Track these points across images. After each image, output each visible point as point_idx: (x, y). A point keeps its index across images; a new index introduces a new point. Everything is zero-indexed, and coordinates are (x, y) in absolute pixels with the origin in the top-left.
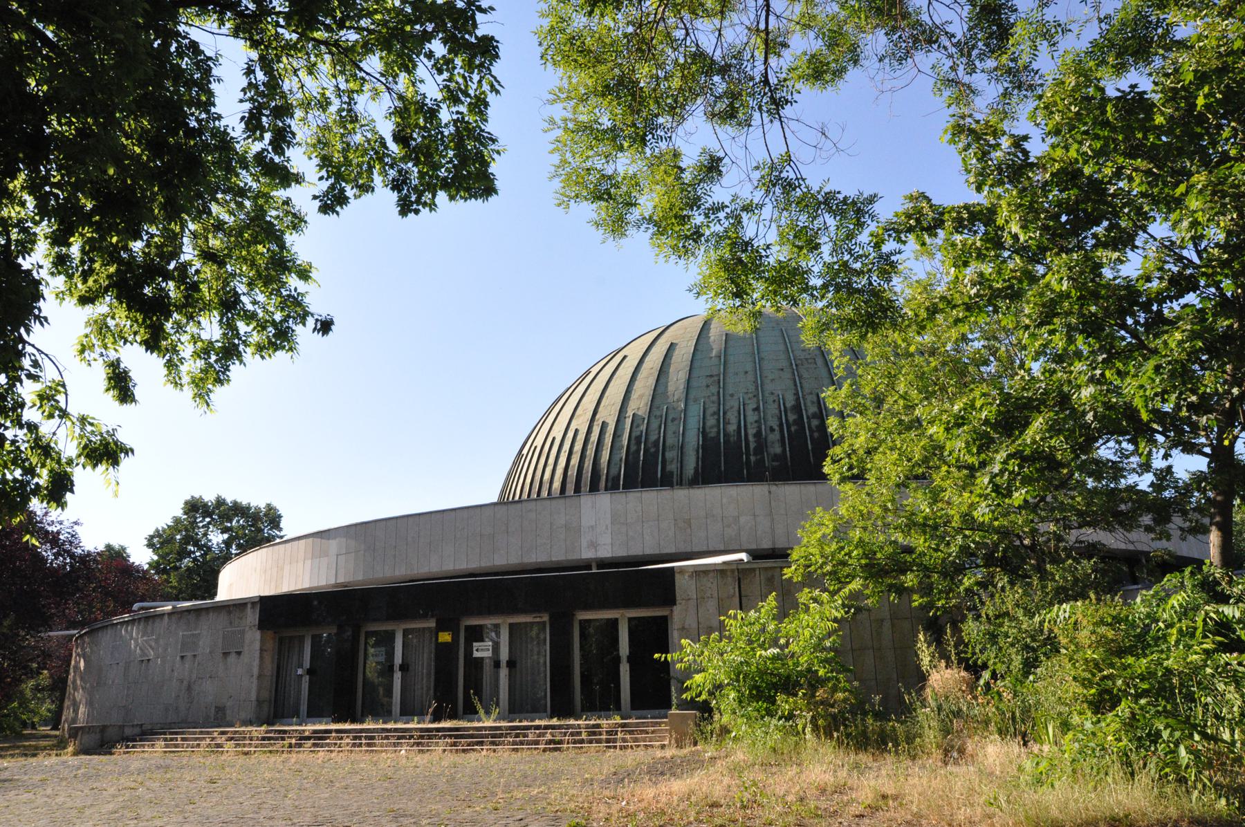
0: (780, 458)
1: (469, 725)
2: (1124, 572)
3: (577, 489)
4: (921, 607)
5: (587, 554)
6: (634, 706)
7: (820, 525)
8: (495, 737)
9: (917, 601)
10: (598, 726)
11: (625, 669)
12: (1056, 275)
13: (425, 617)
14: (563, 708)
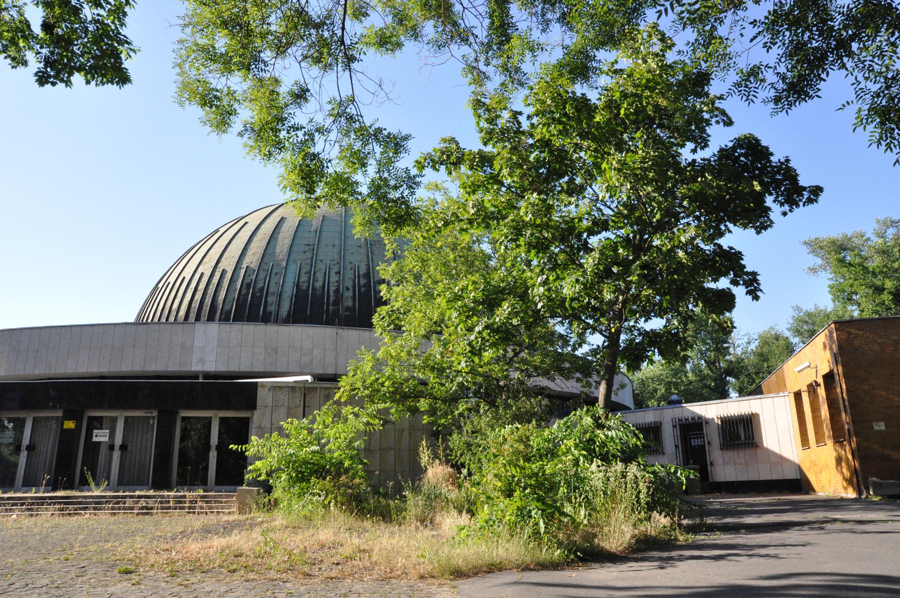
0: (351, 309)
1: (78, 494)
2: (561, 405)
3: (198, 319)
4: (429, 423)
5: (196, 368)
6: (219, 482)
7: (371, 358)
8: (98, 504)
9: (426, 419)
10: (185, 497)
11: (213, 455)
12: (525, 210)
13: (54, 408)
14: (161, 482)
